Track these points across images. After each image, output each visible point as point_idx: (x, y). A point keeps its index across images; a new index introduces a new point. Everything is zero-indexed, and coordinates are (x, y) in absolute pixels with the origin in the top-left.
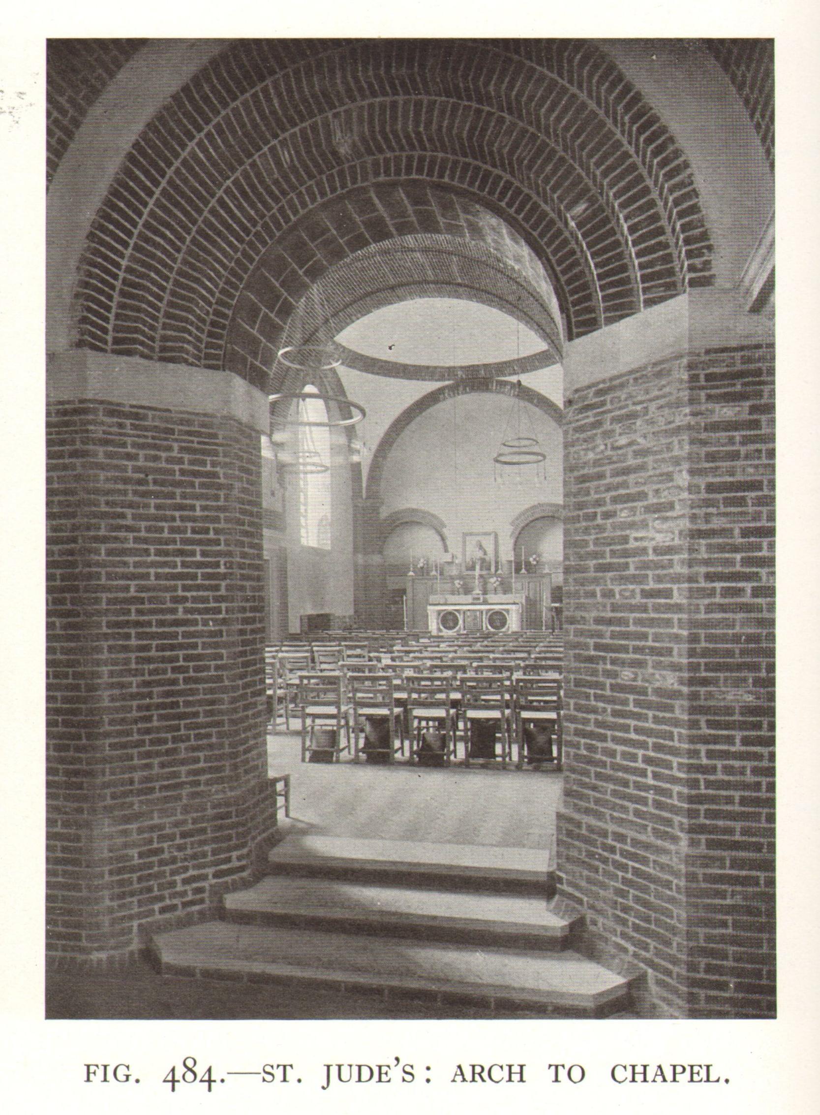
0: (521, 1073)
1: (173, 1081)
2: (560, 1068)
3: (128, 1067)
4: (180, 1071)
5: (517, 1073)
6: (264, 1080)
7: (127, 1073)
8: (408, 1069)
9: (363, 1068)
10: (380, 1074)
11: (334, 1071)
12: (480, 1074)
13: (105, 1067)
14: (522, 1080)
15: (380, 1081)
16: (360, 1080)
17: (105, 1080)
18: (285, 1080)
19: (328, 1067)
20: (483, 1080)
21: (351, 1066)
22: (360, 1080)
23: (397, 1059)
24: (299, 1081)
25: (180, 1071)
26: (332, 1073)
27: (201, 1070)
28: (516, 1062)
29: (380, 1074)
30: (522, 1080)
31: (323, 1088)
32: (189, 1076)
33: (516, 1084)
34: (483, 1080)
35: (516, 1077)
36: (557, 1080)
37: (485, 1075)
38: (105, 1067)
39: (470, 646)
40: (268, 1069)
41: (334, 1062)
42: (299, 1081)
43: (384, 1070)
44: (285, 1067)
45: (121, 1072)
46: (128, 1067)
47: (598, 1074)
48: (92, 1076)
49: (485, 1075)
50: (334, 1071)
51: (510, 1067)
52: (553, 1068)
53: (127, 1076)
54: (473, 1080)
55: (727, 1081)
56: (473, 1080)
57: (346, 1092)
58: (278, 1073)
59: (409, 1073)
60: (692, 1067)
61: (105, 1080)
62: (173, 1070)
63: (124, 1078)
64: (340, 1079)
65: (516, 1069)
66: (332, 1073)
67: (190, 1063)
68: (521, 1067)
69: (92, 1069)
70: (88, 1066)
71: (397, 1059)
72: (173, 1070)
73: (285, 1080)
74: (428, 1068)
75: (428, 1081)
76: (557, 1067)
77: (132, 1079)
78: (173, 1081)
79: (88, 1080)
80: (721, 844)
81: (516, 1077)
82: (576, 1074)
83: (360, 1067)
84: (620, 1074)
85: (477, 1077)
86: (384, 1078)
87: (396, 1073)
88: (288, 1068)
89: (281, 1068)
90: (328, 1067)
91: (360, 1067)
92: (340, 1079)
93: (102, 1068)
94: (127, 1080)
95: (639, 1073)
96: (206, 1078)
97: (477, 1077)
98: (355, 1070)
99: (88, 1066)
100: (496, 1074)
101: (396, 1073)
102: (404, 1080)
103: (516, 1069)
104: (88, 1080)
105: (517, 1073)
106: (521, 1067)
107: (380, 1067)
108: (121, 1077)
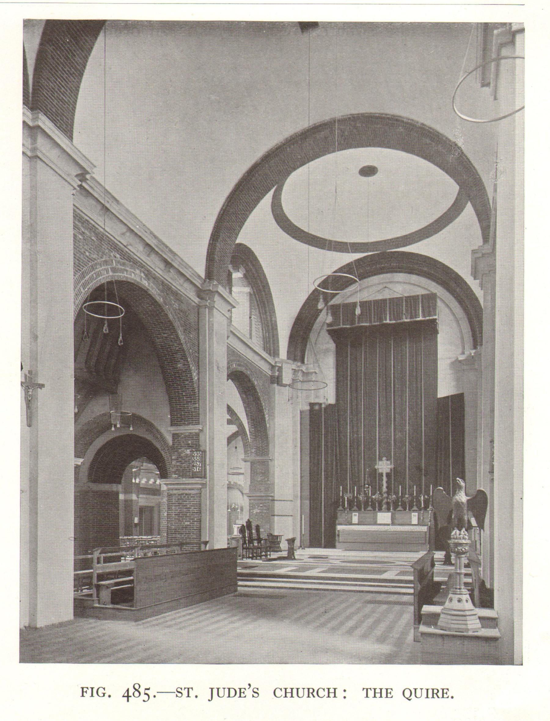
0: (335, 693)
1: (128, 697)
2: (369, 690)
3: (104, 689)
4: (131, 691)
5: (332, 693)
6: (177, 696)
7: (104, 692)
8: (255, 690)
9: (231, 690)
10: (240, 693)
11: (215, 691)
12: (312, 693)
13: (92, 688)
14: (335, 697)
15: (240, 697)
16: (229, 696)
17: (92, 696)
18: (188, 696)
19: (212, 689)
20: (314, 697)
21: (304, 689)
22: (229, 696)
23: (250, 685)
24: (196, 697)
25: (131, 691)
26: (214, 692)
27: (142, 690)
28: (332, 686)
29: (240, 693)
30: (335, 697)
31: (209, 700)
32: (137, 694)
33: (332, 699)
34: (314, 697)
35: (332, 695)
36: (367, 697)
37: (315, 694)
38: (92, 688)
39: (361, 486)
40: (179, 690)
41: (215, 686)
42: (196, 697)
43: (242, 690)
44: (367, 689)
45: (101, 691)
46: (104, 689)
47: (397, 693)
48: (85, 694)
49: (315, 694)
50: (215, 691)
51: (329, 689)
52: (365, 690)
53: (104, 694)
54: (433, 697)
55: (109, 696)
56: (433, 697)
57: (421, 703)
58: (185, 692)
59: (256, 693)
60: (443, 690)
61: (92, 696)
62: (128, 690)
63: (102, 695)
64: (416, 697)
65: (332, 690)
66: (214, 692)
67: (137, 687)
68: (335, 689)
69: (85, 690)
70: (83, 688)
71: (250, 685)
72: (128, 690)
73: (188, 696)
74: (345, 691)
75: (345, 697)
76: (367, 689)
77: (106, 695)
78: (128, 697)
79: (83, 696)
80: (125, 574)
81: (332, 695)
82: (407, 694)
83: (229, 689)
84: (278, 693)
85: (435, 695)
86: (242, 695)
87: (249, 693)
88: (190, 690)
89: (187, 689)
90: (212, 689)
91: (229, 689)
92: (298, 696)
93: (90, 689)
94: (104, 696)
95: (289, 693)
96: (126, 695)
97: (311, 695)
98: (227, 690)
99: (83, 688)
100: (321, 693)
101: (249, 693)
102: (253, 696)
103: (332, 690)
104: (83, 696)
105: (332, 693)
106: (335, 689)
107: (240, 689)
108: (100, 694)
